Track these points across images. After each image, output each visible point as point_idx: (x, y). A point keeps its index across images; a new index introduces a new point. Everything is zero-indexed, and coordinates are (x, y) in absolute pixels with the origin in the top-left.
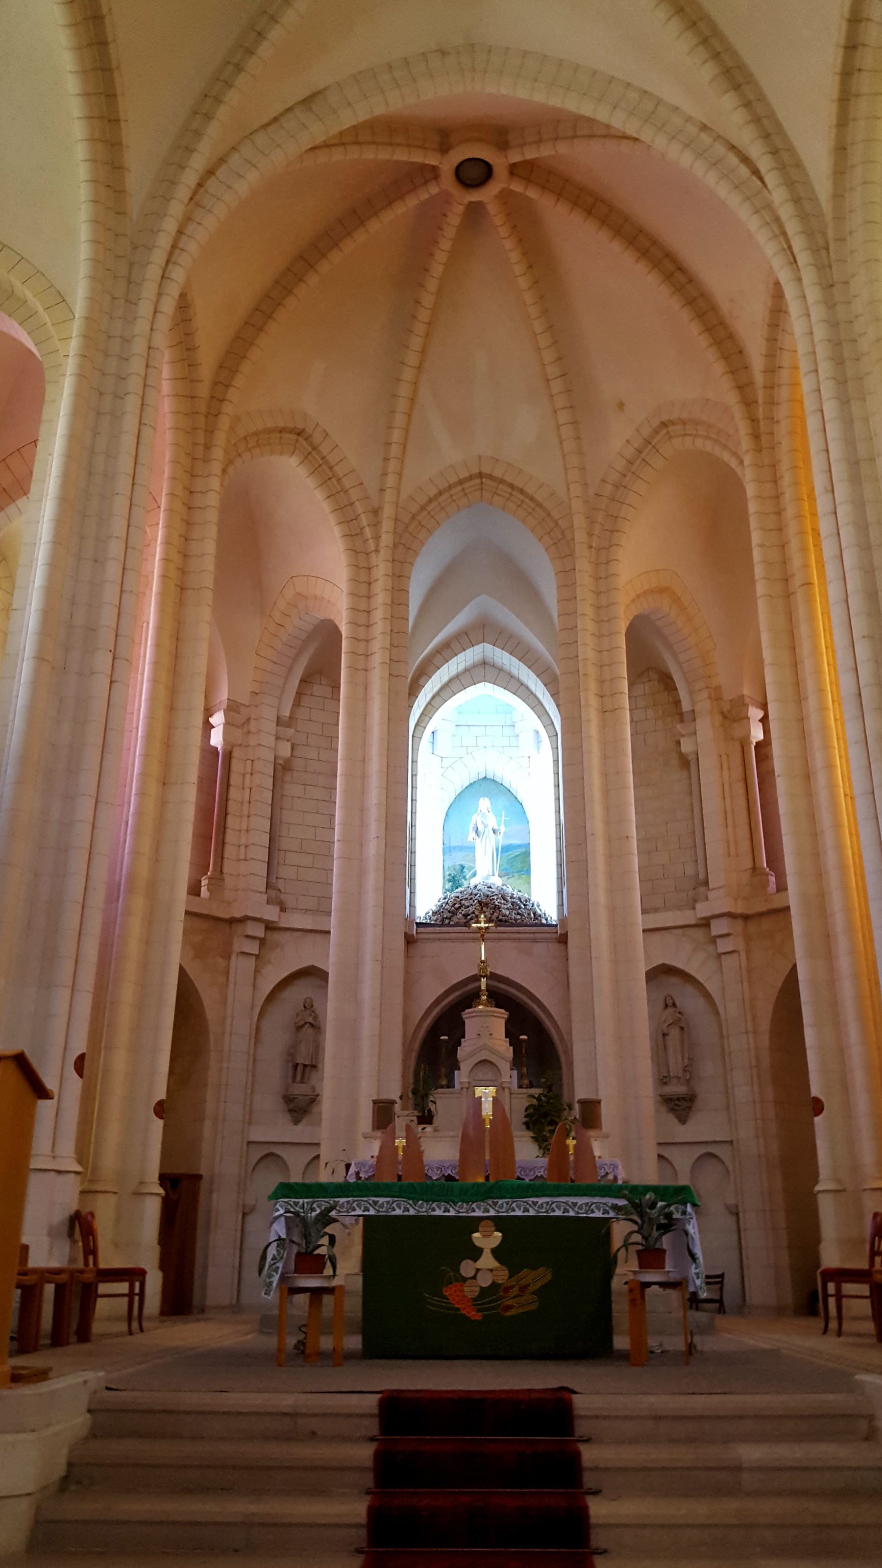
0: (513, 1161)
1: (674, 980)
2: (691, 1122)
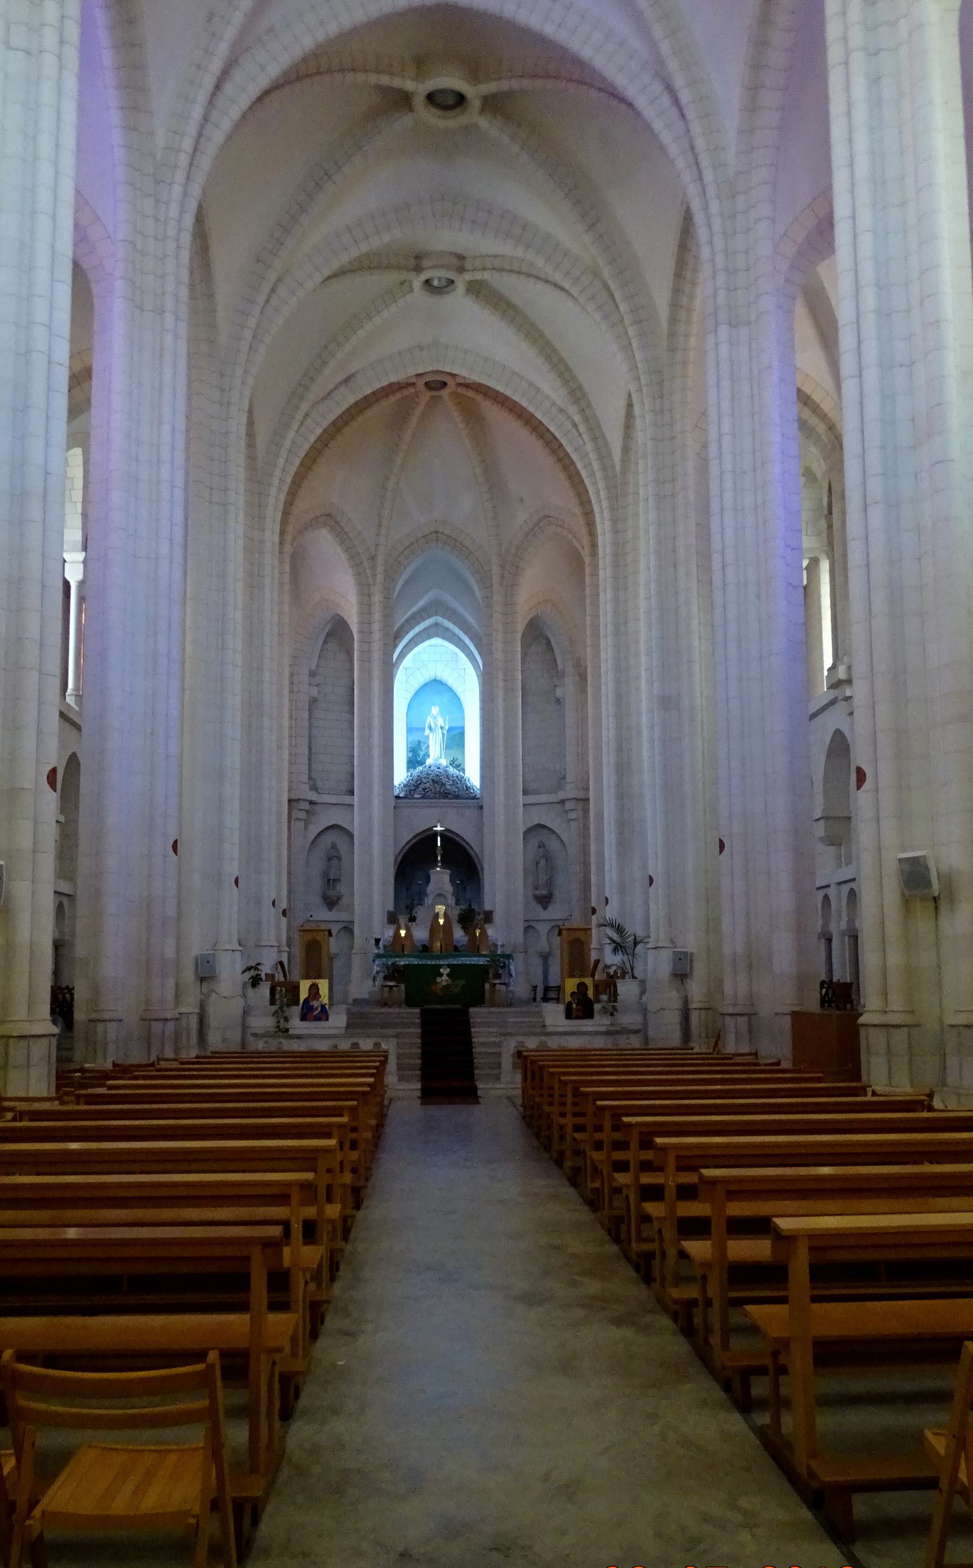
0: (452, 938)
1: (546, 831)
2: (550, 908)
